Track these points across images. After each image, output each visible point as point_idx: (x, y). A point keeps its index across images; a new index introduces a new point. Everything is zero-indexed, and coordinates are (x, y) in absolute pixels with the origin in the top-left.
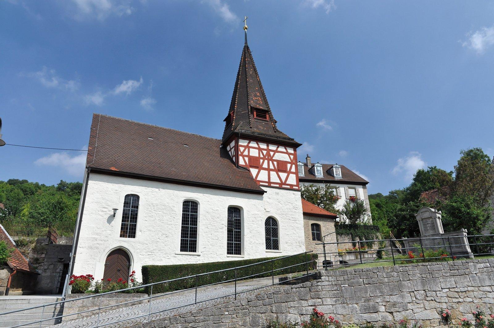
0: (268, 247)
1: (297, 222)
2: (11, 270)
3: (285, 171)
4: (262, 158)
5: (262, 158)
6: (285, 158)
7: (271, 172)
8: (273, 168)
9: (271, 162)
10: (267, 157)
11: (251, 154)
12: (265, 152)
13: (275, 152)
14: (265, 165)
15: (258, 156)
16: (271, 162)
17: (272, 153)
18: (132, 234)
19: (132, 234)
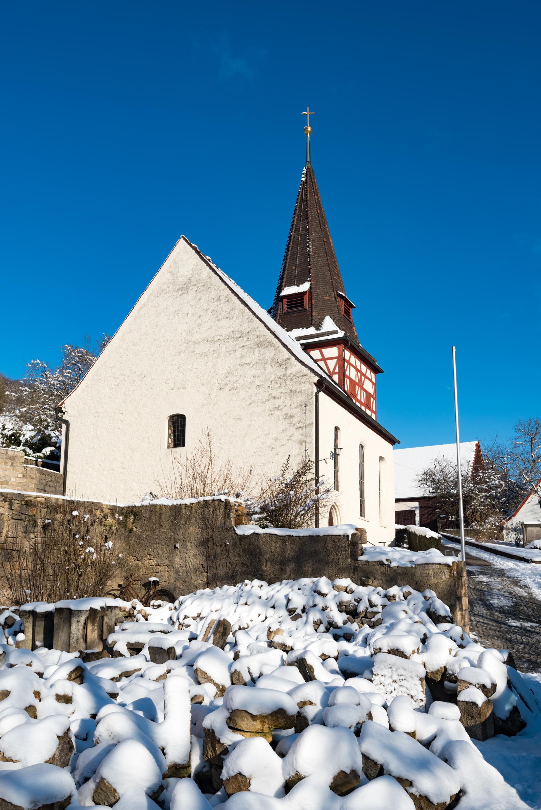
17: (363, 377)
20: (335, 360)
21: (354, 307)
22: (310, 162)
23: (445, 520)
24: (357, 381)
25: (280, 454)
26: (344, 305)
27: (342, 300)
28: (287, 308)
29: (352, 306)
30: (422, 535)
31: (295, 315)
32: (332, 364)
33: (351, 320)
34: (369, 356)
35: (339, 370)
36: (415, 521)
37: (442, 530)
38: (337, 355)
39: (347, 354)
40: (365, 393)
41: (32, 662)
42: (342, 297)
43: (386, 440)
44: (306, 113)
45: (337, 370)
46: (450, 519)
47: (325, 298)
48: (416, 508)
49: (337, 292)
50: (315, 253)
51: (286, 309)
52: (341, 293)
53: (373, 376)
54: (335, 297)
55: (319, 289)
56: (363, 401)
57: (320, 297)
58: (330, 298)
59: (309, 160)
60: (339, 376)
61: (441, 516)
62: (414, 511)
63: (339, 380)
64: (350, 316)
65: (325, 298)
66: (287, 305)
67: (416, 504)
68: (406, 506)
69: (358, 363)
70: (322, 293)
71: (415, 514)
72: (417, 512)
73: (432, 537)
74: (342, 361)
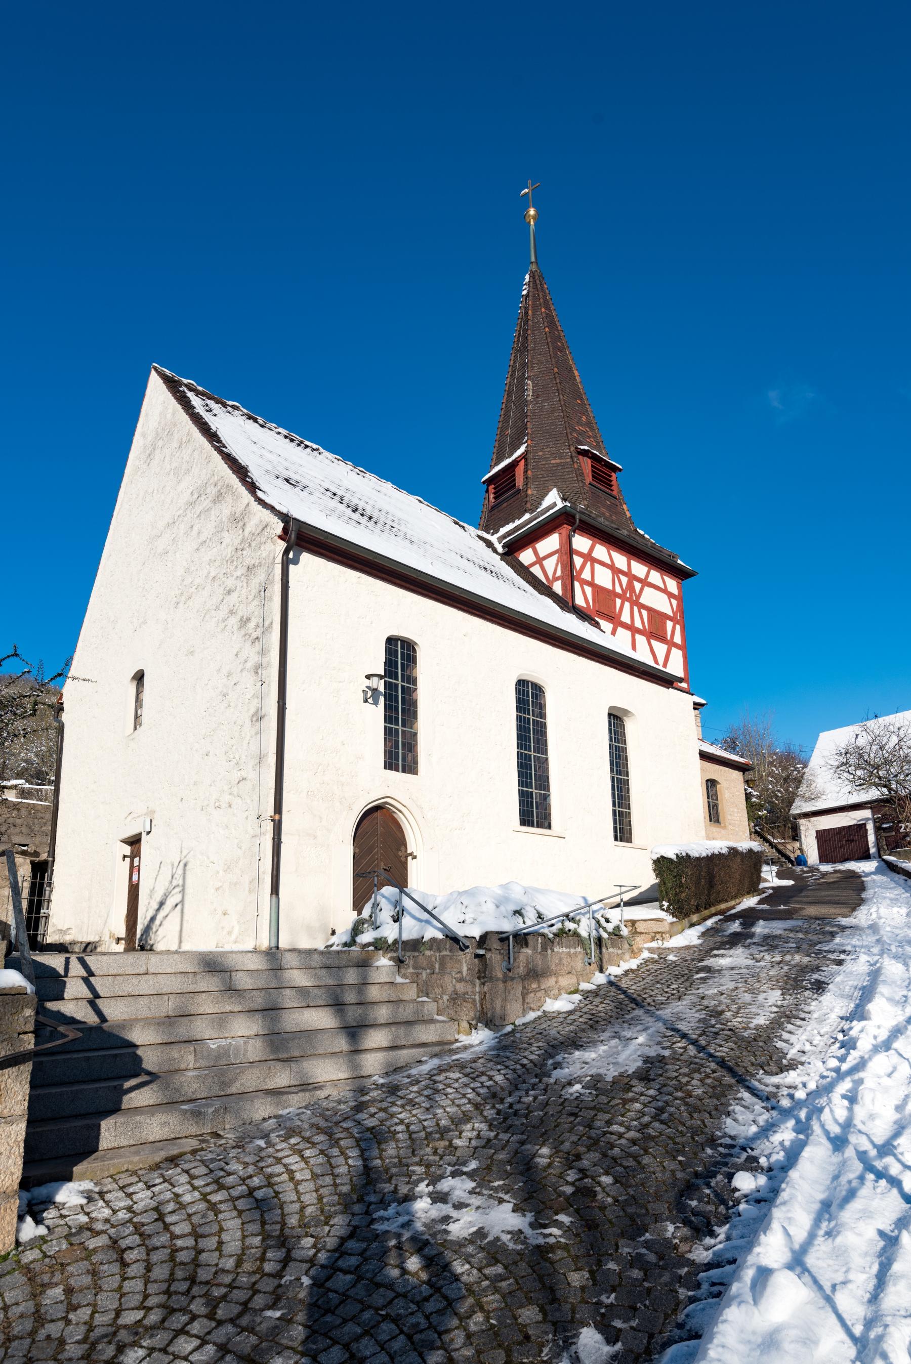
0: (391, 763)
1: (206, 503)
2: (215, 1344)
3: (662, 639)
4: (619, 596)
5: (619, 596)
6: (663, 604)
7: (674, 650)
8: (629, 622)
9: (636, 608)
10: (628, 595)
11: (598, 581)
12: (624, 580)
13: (645, 583)
14: (625, 618)
15: (610, 587)
16: (636, 608)
17: (637, 586)
18: (410, 767)
19: (410, 767)
20: (556, 557)
21: (620, 470)
23: (894, 833)
24: (618, 590)
25: (232, 704)
26: (592, 466)
27: (585, 459)
29: (615, 469)
30: (688, 856)
31: (505, 505)
32: (551, 564)
33: (615, 493)
35: (562, 572)
36: (867, 842)
37: (888, 852)
38: (649, 580)
39: (581, 543)
40: (644, 613)
42: (585, 453)
43: (653, 682)
44: (526, 190)
45: (559, 573)
46: (902, 830)
47: (553, 462)
48: (868, 819)
49: (576, 448)
50: (538, 396)
52: (582, 447)
53: (672, 585)
54: (572, 457)
55: (542, 450)
56: (638, 624)
59: (533, 259)
61: (884, 826)
62: (865, 825)
63: (563, 590)
64: (611, 486)
65: (553, 462)
66: (494, 493)
67: (867, 813)
68: (848, 819)
69: (655, 577)
71: (866, 831)
72: (870, 827)
73: (662, 857)
74: (567, 552)
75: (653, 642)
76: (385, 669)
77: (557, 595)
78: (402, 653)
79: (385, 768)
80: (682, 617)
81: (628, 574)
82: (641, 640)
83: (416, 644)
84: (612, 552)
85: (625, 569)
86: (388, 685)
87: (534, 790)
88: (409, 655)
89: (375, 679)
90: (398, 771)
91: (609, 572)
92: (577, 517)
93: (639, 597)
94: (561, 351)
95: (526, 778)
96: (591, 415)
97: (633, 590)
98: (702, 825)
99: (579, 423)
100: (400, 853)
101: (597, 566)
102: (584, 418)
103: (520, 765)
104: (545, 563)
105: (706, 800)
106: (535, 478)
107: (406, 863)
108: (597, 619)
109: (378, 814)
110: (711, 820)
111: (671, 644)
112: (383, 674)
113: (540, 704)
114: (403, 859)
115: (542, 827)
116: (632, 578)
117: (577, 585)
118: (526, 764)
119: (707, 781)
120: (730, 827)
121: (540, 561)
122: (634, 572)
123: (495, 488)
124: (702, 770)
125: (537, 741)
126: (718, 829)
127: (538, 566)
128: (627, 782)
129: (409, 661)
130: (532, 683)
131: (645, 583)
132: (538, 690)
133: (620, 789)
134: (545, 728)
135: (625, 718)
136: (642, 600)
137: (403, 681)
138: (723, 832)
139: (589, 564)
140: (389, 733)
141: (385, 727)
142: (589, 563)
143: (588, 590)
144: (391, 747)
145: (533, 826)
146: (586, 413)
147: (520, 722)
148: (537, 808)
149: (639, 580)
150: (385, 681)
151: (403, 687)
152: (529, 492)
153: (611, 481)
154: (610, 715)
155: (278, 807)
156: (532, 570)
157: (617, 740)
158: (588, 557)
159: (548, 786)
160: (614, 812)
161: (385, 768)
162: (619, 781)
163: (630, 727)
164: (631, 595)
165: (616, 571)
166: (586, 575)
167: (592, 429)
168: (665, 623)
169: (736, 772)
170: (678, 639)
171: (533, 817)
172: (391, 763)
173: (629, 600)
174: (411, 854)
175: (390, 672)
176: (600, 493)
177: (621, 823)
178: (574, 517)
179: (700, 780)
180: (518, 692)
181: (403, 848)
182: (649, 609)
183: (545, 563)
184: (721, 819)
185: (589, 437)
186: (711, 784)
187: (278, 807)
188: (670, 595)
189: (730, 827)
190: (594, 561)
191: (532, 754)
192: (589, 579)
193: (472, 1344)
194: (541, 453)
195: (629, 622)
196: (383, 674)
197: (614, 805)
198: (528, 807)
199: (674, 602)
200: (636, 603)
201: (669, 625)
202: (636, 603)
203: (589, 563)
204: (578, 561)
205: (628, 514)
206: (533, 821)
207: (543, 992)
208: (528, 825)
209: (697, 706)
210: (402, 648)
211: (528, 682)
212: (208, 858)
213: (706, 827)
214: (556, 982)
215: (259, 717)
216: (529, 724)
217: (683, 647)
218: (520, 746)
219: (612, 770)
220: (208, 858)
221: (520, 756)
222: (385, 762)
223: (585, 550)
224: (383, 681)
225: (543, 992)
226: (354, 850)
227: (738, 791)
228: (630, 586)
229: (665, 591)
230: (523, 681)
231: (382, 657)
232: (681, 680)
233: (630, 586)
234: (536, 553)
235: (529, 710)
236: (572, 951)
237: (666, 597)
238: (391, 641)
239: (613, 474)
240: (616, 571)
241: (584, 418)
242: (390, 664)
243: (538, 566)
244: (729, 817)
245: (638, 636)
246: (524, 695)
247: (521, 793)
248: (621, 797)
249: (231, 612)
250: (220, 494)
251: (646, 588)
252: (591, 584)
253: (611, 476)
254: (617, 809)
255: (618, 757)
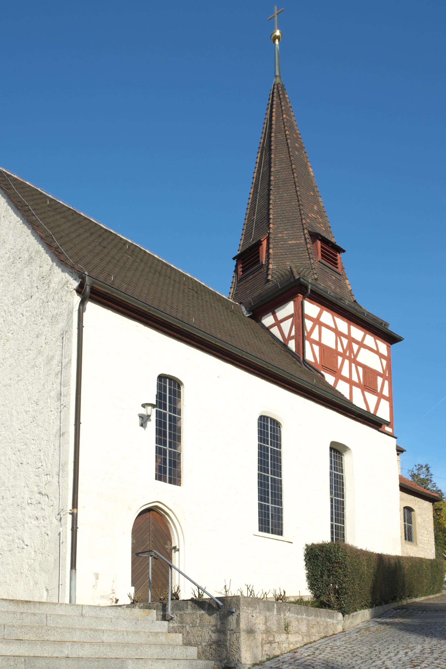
0: (160, 476)
3: (374, 391)
4: (340, 354)
5: (340, 354)
7: (383, 401)
8: (348, 377)
10: (348, 354)
11: (323, 342)
14: (345, 372)
15: (334, 347)
16: (353, 365)
17: (355, 347)
20: (291, 320)
22: (280, 76)
24: (340, 350)
28: (242, 271)
31: (251, 277)
32: (286, 326)
33: (339, 270)
34: (376, 319)
40: (360, 369)
41: (116, 599)
45: (293, 333)
51: (241, 273)
53: (383, 347)
54: (305, 239)
56: (355, 378)
57: (282, 243)
58: (298, 242)
59: (277, 73)
60: (295, 341)
65: (290, 242)
69: (370, 340)
70: (285, 238)
75: (366, 393)
76: (157, 401)
77: (292, 351)
78: (170, 389)
79: (156, 479)
80: (390, 374)
81: (348, 337)
82: (357, 391)
83: (182, 384)
84: (335, 318)
85: (346, 333)
86: (159, 414)
87: (270, 505)
88: (175, 391)
89: (149, 408)
90: (166, 482)
91: (333, 334)
92: (310, 287)
93: (356, 356)
94: (298, 151)
95: (265, 494)
96: (322, 204)
97: (351, 350)
98: (399, 542)
99: (312, 211)
100: (167, 547)
101: (323, 328)
102: (316, 208)
103: (260, 454)
104: (282, 325)
105: (403, 523)
106: (275, 254)
107: (171, 554)
108: (322, 372)
109: (151, 514)
110: (406, 539)
111: (381, 396)
112: (155, 403)
113: (277, 436)
114: (168, 551)
115: (275, 534)
116: (351, 340)
117: (307, 343)
118: (265, 490)
119: (405, 508)
120: (421, 545)
121: (278, 323)
122: (353, 335)
123: (242, 268)
124: (401, 499)
125: (273, 466)
126: (411, 547)
127: (276, 327)
128: (343, 503)
129: (175, 395)
130: (271, 419)
131: (361, 345)
132: (276, 424)
133: (337, 508)
134: (280, 456)
135: (344, 454)
136: (359, 359)
137: (170, 411)
138: (415, 548)
139: (317, 327)
140: (159, 452)
141: (156, 447)
142: (317, 326)
143: (316, 348)
144: (161, 463)
145: (268, 532)
146: (317, 203)
147: (261, 449)
148: (272, 519)
149: (357, 342)
150: (157, 410)
151: (170, 416)
152: (271, 266)
153: (336, 260)
154: (331, 449)
155: (75, 504)
156: (272, 330)
157: (336, 469)
158: (317, 321)
159: (281, 502)
160: (332, 526)
161: (156, 479)
162: (337, 501)
163: (347, 459)
164: (350, 354)
165: (338, 334)
166: (315, 336)
167: (322, 217)
168: (376, 379)
169: (428, 502)
170: (386, 392)
171: (269, 525)
172: (160, 476)
173: (349, 358)
174: (175, 548)
175: (160, 403)
176: (327, 270)
177: (337, 535)
178: (306, 288)
179: (399, 507)
180: (260, 425)
181: (169, 542)
182: (364, 367)
183: (282, 325)
184: (414, 539)
185: (320, 223)
186: (408, 510)
187: (75, 504)
188: (381, 356)
189: (421, 545)
190: (321, 324)
191: (270, 475)
192: (317, 339)
193: (1, 514)
194: (280, 235)
195: (348, 377)
196: (155, 403)
197: (332, 520)
198: (265, 517)
199: (384, 362)
200: (353, 361)
201: (380, 380)
202: (353, 361)
203: (317, 326)
204: (308, 324)
205: (350, 288)
206: (269, 529)
207: (277, 644)
208: (265, 532)
209: (400, 451)
210: (170, 384)
211: (267, 417)
212: (23, 542)
213: (402, 544)
214: (287, 638)
215: (61, 434)
216: (268, 452)
217: (389, 399)
218: (260, 469)
219: (331, 493)
220: (23, 542)
221: (260, 476)
222: (156, 475)
223: (315, 316)
224: (155, 409)
225: (277, 644)
226: (132, 541)
227: (428, 517)
228: (350, 347)
229: (377, 352)
230: (264, 417)
231: (154, 391)
232: (388, 424)
233: (350, 347)
234: (275, 318)
235: (268, 440)
236: (299, 617)
237: (377, 357)
238: (162, 378)
239: (338, 254)
240: (338, 334)
241: (316, 208)
242: (160, 396)
243: (276, 327)
244: (420, 538)
245: (354, 388)
246: (264, 429)
247: (261, 507)
248: (337, 515)
249: (40, 352)
250: (31, 258)
251: (362, 349)
252: (319, 343)
253: (336, 256)
254: (334, 523)
255: (336, 482)
